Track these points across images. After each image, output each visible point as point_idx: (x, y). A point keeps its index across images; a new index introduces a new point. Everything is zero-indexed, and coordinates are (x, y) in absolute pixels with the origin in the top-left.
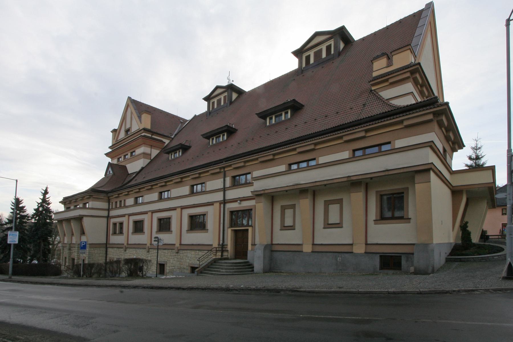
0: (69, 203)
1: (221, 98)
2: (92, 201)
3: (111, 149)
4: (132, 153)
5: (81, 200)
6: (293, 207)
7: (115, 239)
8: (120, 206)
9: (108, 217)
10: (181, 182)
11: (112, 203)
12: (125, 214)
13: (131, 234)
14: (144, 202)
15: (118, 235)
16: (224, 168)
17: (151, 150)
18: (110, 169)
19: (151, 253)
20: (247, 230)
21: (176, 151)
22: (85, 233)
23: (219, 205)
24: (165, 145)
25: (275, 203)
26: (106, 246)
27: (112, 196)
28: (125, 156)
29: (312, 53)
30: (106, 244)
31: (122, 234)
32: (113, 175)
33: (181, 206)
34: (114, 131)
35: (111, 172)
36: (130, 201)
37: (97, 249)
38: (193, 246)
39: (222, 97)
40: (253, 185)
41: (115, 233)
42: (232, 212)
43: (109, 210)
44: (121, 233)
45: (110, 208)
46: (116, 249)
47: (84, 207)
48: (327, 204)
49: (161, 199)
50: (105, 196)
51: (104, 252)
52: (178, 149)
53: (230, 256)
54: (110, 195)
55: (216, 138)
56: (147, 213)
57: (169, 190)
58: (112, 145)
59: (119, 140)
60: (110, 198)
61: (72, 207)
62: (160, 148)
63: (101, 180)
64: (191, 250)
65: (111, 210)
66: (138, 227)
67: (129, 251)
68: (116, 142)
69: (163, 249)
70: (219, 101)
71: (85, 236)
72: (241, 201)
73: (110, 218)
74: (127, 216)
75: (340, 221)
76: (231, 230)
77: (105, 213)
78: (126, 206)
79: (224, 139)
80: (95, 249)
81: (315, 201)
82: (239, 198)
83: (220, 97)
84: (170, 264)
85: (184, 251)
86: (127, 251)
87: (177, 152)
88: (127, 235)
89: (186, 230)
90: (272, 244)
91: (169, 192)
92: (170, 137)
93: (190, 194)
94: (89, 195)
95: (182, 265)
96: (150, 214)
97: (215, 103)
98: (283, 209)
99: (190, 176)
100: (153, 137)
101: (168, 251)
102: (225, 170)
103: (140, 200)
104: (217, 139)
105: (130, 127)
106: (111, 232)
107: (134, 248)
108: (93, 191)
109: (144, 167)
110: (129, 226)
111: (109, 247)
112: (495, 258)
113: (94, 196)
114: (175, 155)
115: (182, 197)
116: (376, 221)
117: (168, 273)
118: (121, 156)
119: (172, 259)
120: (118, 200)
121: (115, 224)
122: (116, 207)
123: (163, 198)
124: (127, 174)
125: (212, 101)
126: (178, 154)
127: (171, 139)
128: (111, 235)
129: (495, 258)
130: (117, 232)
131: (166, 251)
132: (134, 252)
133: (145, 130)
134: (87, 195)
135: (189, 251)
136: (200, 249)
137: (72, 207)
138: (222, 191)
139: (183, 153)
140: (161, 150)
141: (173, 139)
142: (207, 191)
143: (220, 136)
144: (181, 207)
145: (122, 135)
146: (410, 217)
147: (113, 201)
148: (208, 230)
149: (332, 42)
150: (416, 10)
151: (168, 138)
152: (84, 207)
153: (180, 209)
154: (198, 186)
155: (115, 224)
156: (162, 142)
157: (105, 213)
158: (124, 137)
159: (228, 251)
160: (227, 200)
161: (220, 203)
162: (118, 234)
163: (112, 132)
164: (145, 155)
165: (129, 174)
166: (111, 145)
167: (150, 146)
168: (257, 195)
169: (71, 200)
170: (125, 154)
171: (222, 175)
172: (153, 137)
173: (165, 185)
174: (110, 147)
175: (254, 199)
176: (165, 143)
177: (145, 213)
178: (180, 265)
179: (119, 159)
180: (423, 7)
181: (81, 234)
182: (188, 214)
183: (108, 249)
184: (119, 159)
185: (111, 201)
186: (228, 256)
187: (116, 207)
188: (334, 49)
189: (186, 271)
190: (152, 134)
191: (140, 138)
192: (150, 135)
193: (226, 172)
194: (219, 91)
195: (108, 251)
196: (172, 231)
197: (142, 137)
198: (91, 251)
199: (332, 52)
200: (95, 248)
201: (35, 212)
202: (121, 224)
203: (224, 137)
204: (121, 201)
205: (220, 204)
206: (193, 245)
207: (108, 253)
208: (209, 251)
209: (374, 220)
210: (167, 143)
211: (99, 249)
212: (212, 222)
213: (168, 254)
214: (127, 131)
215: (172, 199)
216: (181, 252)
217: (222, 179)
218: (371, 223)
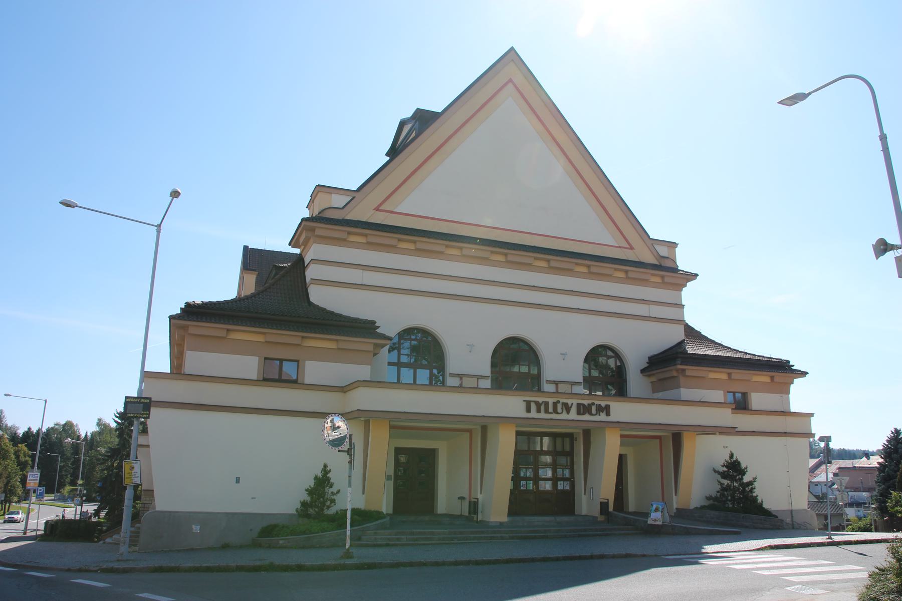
112: (281, 542)
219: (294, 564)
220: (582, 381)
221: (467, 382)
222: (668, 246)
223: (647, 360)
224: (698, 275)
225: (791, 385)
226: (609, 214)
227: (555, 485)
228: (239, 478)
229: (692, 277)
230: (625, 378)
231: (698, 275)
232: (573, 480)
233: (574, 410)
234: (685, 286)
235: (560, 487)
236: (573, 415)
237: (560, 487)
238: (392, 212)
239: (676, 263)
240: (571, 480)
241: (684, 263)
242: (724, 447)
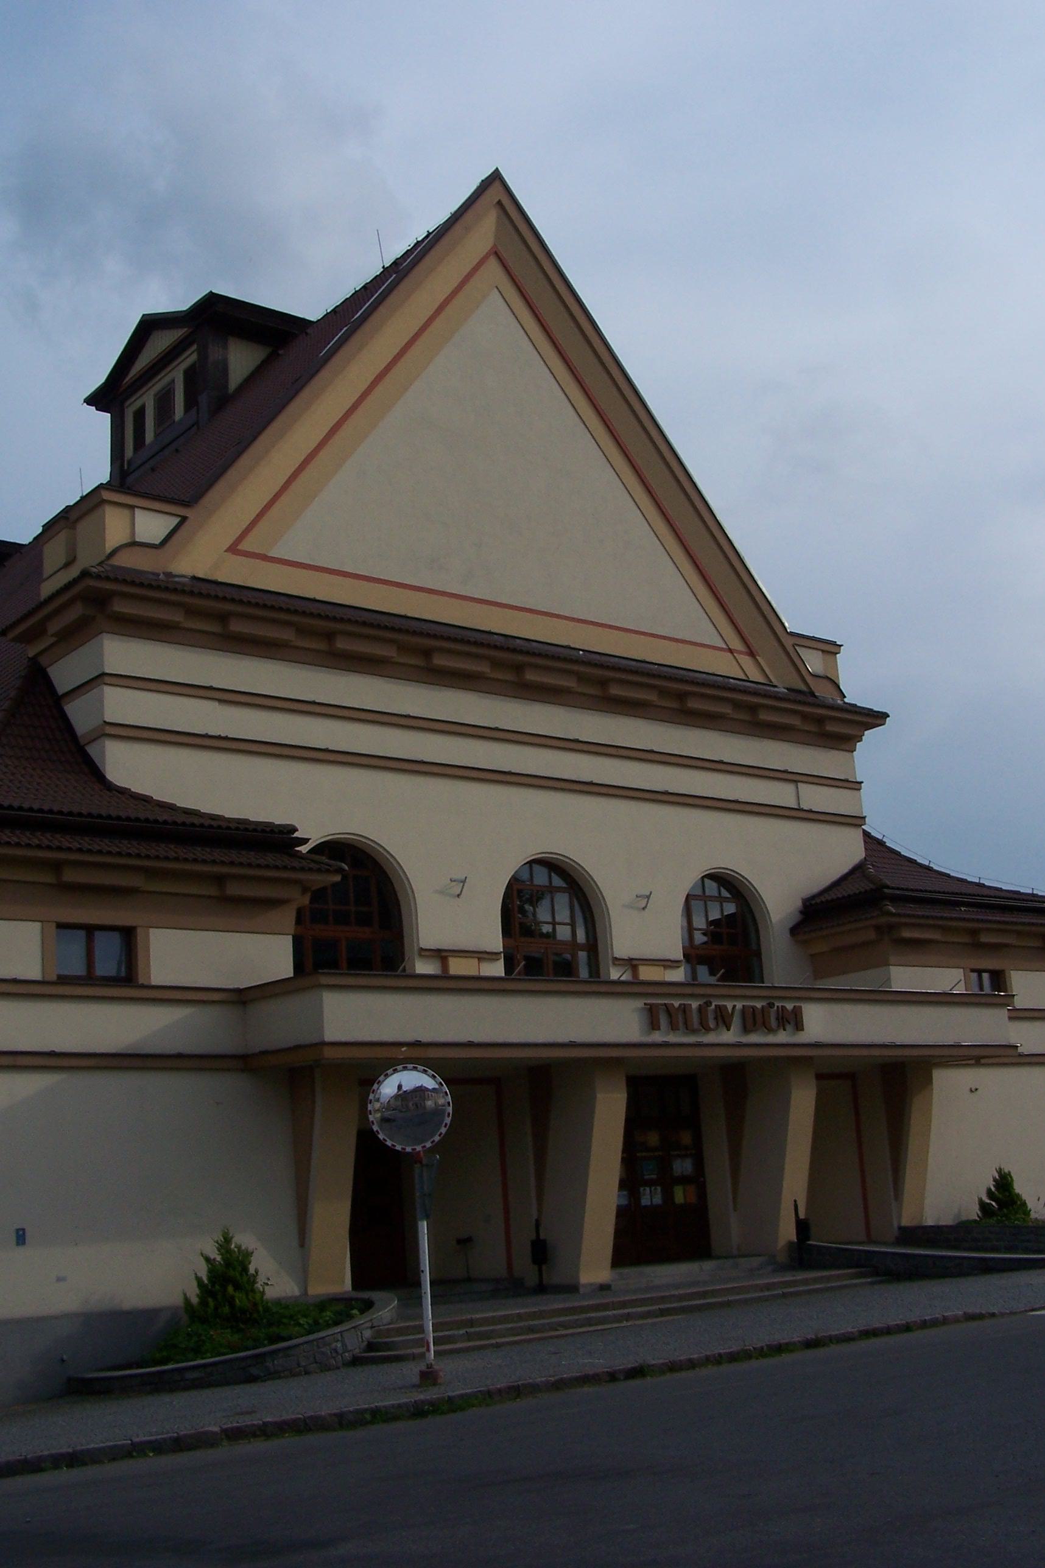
1: (173, 381)
39: (176, 375)
63: (357, 1144)
70: (164, 401)
83: (167, 380)
97: (147, 412)
146: (864, 815)
189: (528, 883)
194: (161, 342)
201: (5, 564)
219: (46, 1453)
220: (682, 958)
221: (457, 967)
222: (823, 651)
223: (799, 904)
224: (888, 716)
226: (149, 544)
227: (668, 1195)
228: (23, 1230)
230: (754, 947)
231: (888, 716)
232: (702, 1179)
233: (736, 1022)
234: (863, 735)
235: (645, 1201)
236: (730, 1036)
237: (645, 1201)
238: (265, 558)
240: (697, 1180)
242: (971, 1091)
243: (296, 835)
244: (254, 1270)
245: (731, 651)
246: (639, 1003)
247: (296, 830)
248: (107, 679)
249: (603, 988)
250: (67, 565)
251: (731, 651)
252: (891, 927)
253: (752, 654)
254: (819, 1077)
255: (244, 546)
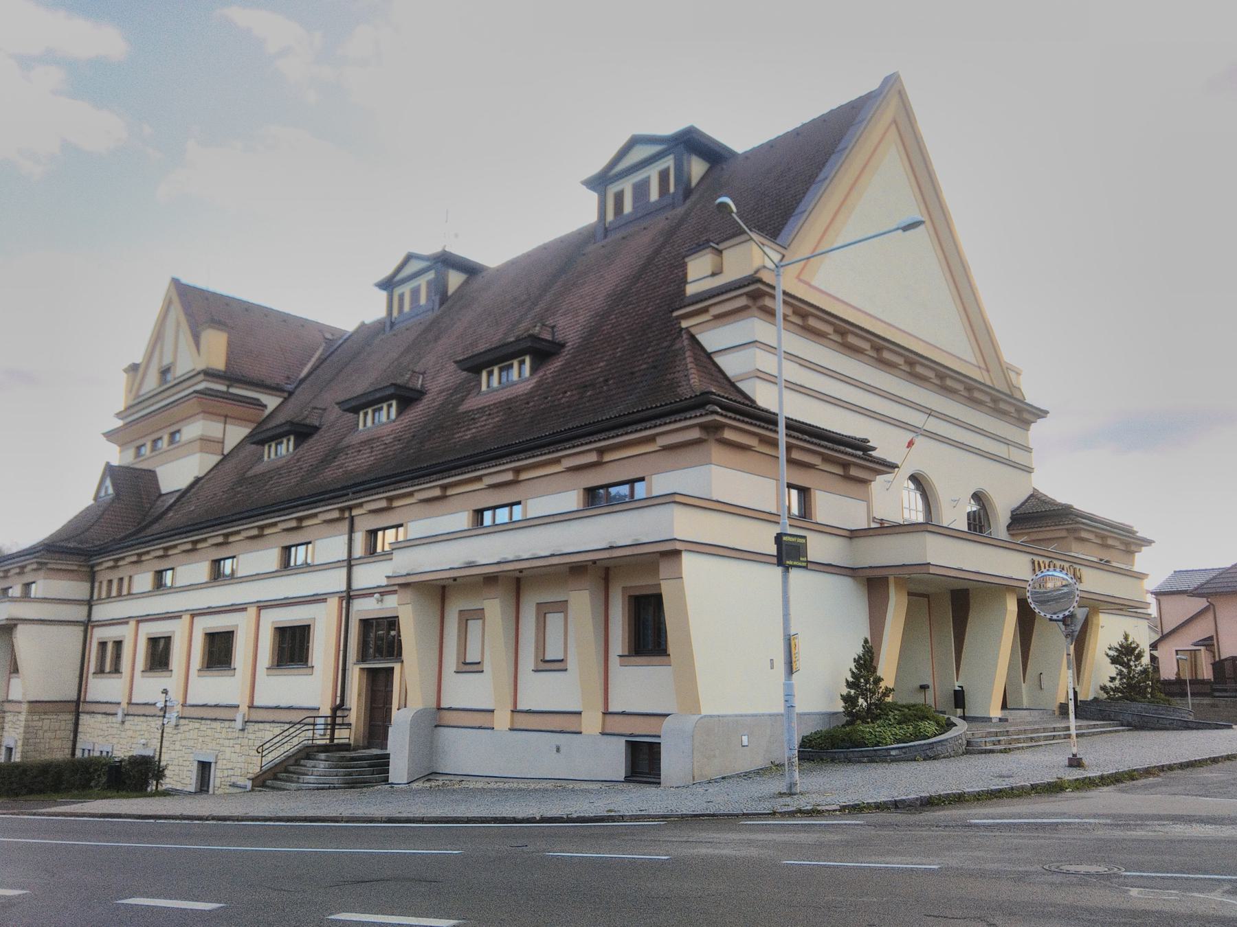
0: (17, 574)
2: (45, 578)
3: (122, 419)
4: (173, 435)
5: (19, 574)
6: (562, 607)
7: (102, 689)
8: (120, 595)
9: (88, 625)
10: (443, 498)
11: (101, 582)
12: (130, 617)
13: (196, 672)
14: (313, 561)
15: (108, 675)
16: (350, 508)
17: (225, 428)
18: (108, 482)
19: (182, 729)
20: (392, 669)
21: (379, 406)
22: (20, 671)
23: (339, 602)
24: (267, 412)
25: (447, 601)
26: (77, 707)
27: (100, 563)
28: (155, 441)
29: (627, 186)
30: (78, 702)
31: (118, 675)
32: (113, 501)
33: (257, 602)
34: (134, 368)
35: (111, 491)
36: (143, 581)
37: (51, 717)
38: (204, 709)
39: (422, 282)
40: (391, 559)
41: (101, 671)
42: (366, 624)
43: (90, 603)
44: (116, 670)
45: (95, 597)
46: (99, 716)
47: (26, 596)
48: (543, 611)
49: (217, 575)
50: (82, 564)
51: (71, 726)
52: (286, 434)
53: (355, 740)
54: (94, 562)
55: (501, 370)
56: (244, 609)
57: (310, 543)
58: (128, 408)
59: (143, 395)
60: (96, 569)
61: (16, 591)
62: (250, 421)
64: (273, 722)
65: (96, 603)
66: (159, 653)
67: (132, 723)
68: (134, 399)
69: (211, 720)
70: (415, 293)
71: (19, 678)
72: (382, 594)
73: (93, 627)
74: (132, 623)
75: (564, 656)
76: (360, 668)
77: (80, 613)
78: (132, 594)
79: (522, 375)
80: (43, 717)
81: (610, 598)
82: (379, 587)
84: (225, 762)
85: (257, 726)
86: (127, 725)
87: (381, 409)
88: (128, 679)
89: (267, 666)
90: (439, 709)
91: (235, 559)
92: (282, 390)
93: (364, 558)
94: (37, 563)
95: (251, 766)
96: (252, 611)
98: (543, 611)
99: (179, 547)
100: (232, 390)
101: (223, 725)
102: (353, 514)
103: (299, 555)
104: (504, 374)
105: (171, 363)
106: (92, 665)
107: (144, 715)
108: (48, 551)
109: (201, 476)
110: (136, 653)
111: (82, 713)
112: (893, 753)
113: (50, 566)
114: (377, 414)
115: (262, 577)
116: (623, 658)
117: (219, 788)
118: (145, 442)
119: (230, 748)
120: (114, 575)
121: (103, 645)
122: (109, 596)
123: (292, 563)
124: (157, 494)
125: (397, 291)
126: (284, 446)
127: (286, 395)
128: (90, 676)
129: (893, 753)
130: (107, 669)
131: (217, 725)
132: (144, 727)
133: (209, 374)
134: (31, 561)
135: (267, 726)
136: (205, 717)
137: (16, 591)
138: (344, 567)
139: (296, 446)
140: (254, 425)
141: (291, 394)
142: (315, 564)
143: (511, 366)
144: (259, 604)
145: (151, 382)
147: (103, 577)
148: (313, 667)
149: (669, 162)
150: (854, 96)
151: (278, 393)
152: (26, 596)
153: (189, 616)
154: (387, 532)
155: (103, 645)
156: (260, 405)
157: (80, 613)
158: (155, 389)
159: (350, 724)
160: (96, 621)
161: (340, 597)
162: (109, 673)
163: (126, 371)
164: (205, 443)
165: (161, 495)
166: (123, 409)
167: (223, 418)
168: (404, 585)
169: (8, 571)
170: (155, 436)
171: (345, 526)
172: (232, 390)
173: (389, 509)
174: (119, 415)
175: (395, 592)
176: (265, 406)
177: (175, 616)
178: (246, 764)
179: (139, 448)
180: (874, 85)
181: (10, 673)
182: (204, 629)
183: (80, 717)
184: (139, 448)
185: (99, 577)
186: (349, 738)
187: (109, 596)
188: (669, 179)
190: (227, 383)
191: (193, 398)
192: (223, 388)
193: (355, 518)
195: (81, 722)
196: (171, 671)
197: (198, 395)
198: (30, 723)
199: (672, 189)
200: (45, 713)
202: (118, 644)
203: (491, 377)
204: (121, 579)
205: (341, 599)
206: (277, 708)
207: (80, 729)
208: (293, 724)
209: (620, 656)
210: (271, 407)
211: (55, 717)
212: (322, 648)
213: (221, 733)
214: (165, 372)
215: (317, 568)
216: (251, 727)
217: (346, 537)
218: (614, 661)
223: (1009, 515)
225: (1136, 554)
229: (1042, 414)
231: (1048, 413)
239: (1020, 390)
241: (1032, 395)
243: (868, 444)
244: (116, 419)
245: (979, 367)
246: (1028, 558)
247: (869, 442)
248: (759, 345)
249: (236, 581)
250: (713, 274)
251: (979, 367)
252: (1075, 530)
253: (988, 371)
254: (910, 594)
255: (893, 127)
